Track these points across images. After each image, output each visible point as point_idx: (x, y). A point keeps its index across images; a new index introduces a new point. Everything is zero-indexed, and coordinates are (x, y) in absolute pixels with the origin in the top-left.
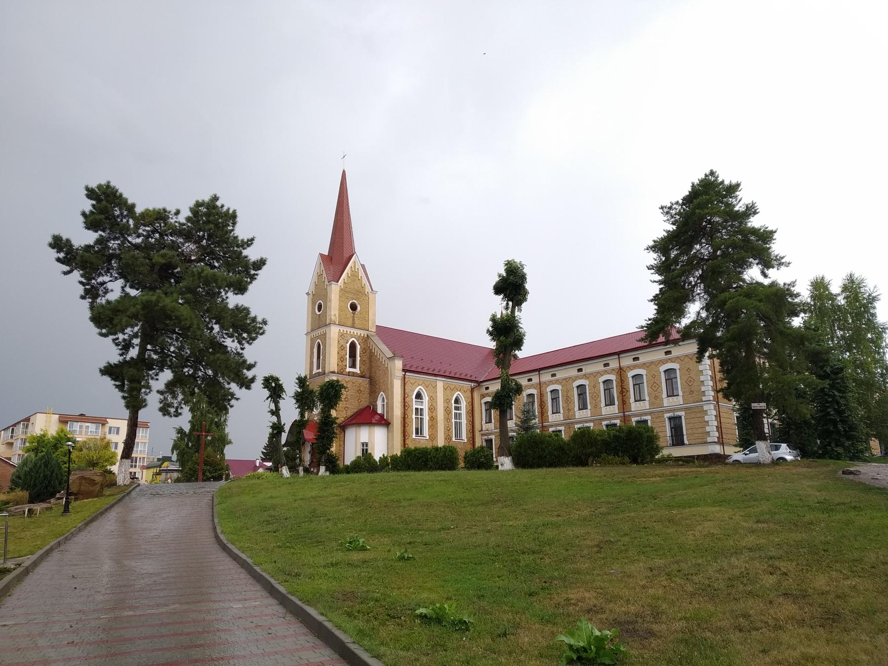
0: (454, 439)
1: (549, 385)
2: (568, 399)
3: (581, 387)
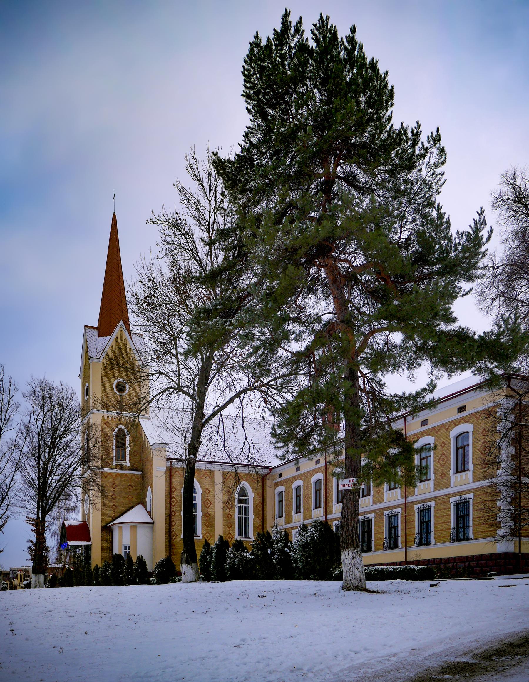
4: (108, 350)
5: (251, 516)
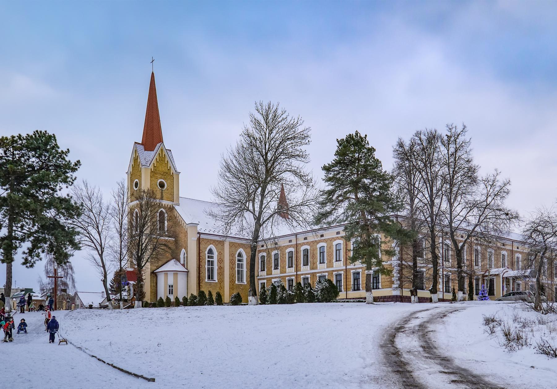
0: (237, 282)
1: (302, 245)
3: (306, 251)
4: (154, 161)
5: (245, 269)
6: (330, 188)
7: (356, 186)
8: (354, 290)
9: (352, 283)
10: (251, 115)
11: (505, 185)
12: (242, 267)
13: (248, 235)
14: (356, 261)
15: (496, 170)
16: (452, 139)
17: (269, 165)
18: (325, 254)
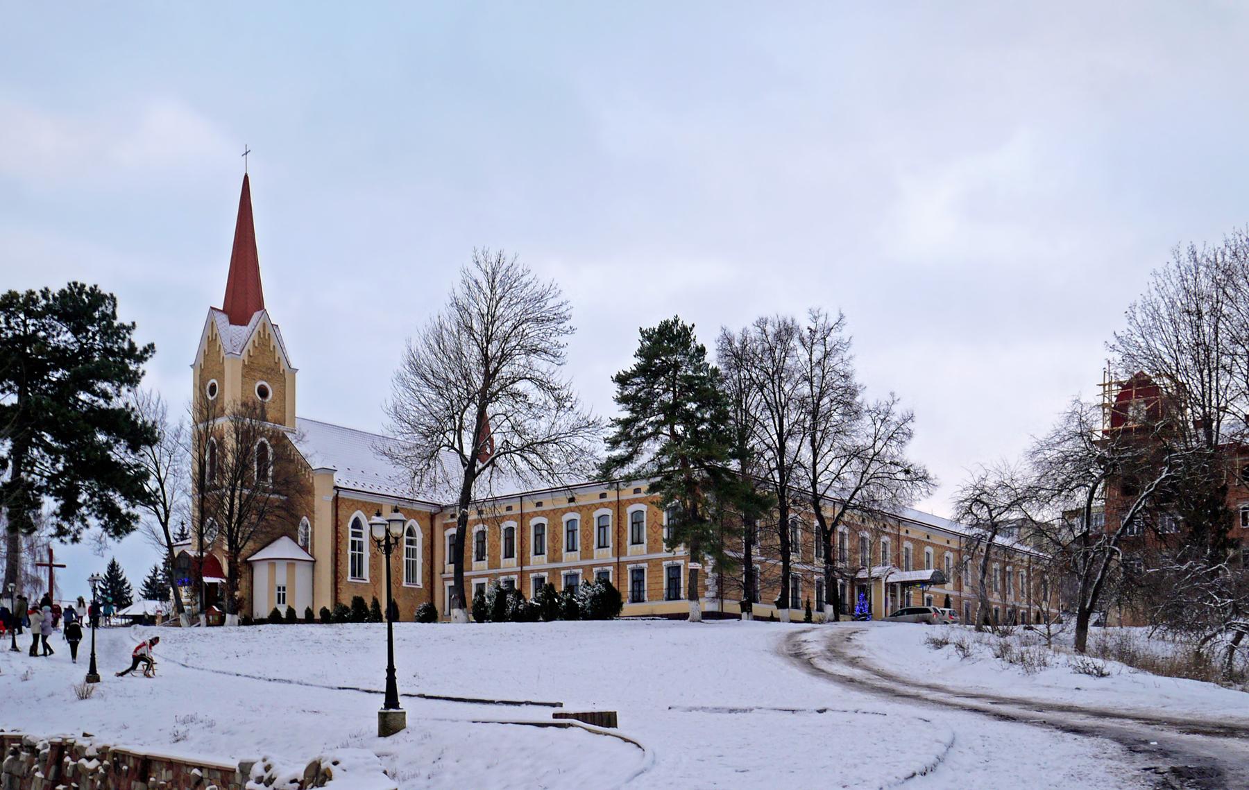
0: (404, 584)
2: (555, 538)
3: (540, 527)
4: (249, 345)
5: (419, 560)
6: (626, 415)
7: (673, 412)
8: (669, 599)
9: (629, 588)
10: (465, 271)
11: (905, 421)
12: (414, 556)
13: (1084, 504)
14: (676, 546)
15: (892, 394)
16: (818, 336)
17: (494, 365)
18: (578, 534)
